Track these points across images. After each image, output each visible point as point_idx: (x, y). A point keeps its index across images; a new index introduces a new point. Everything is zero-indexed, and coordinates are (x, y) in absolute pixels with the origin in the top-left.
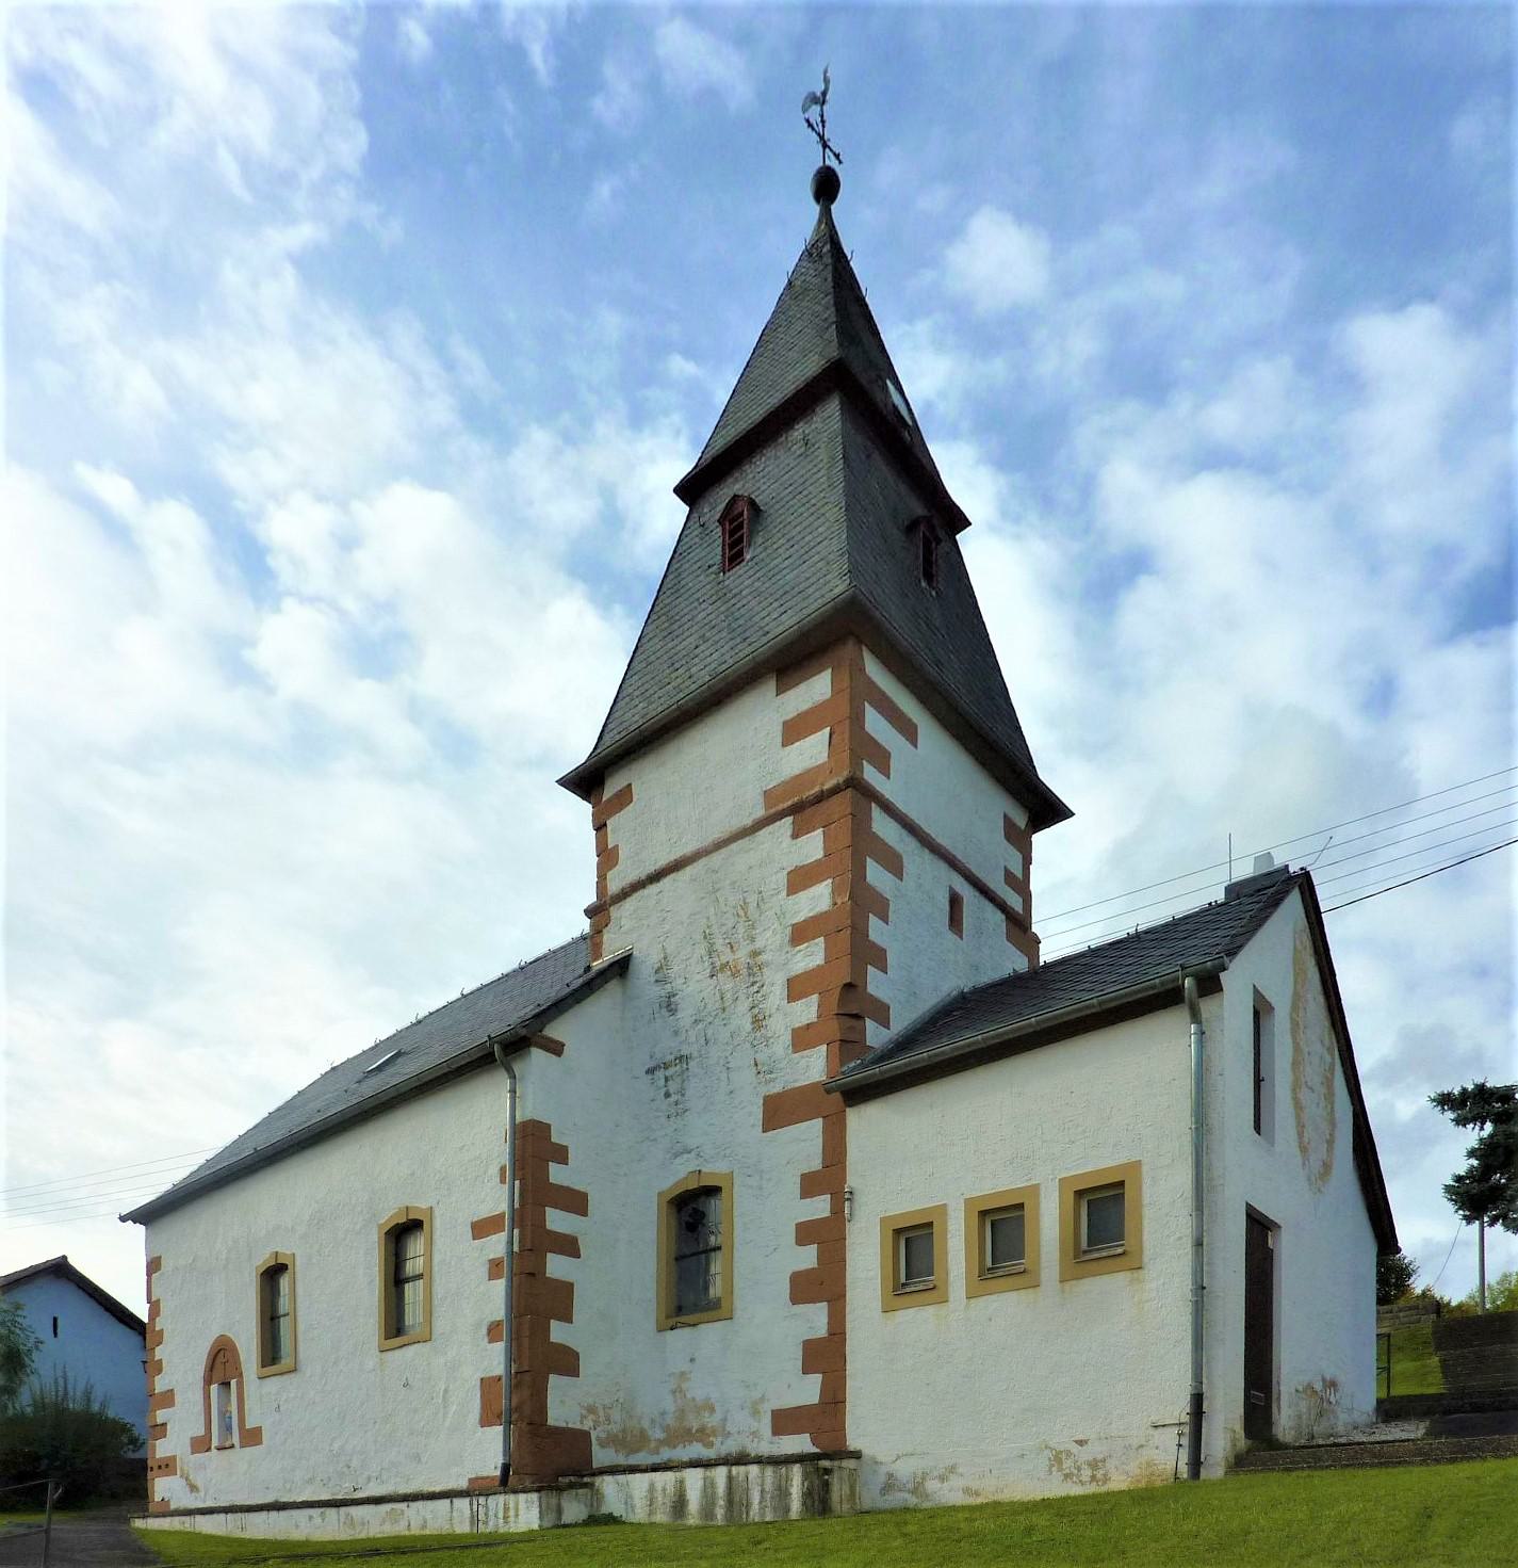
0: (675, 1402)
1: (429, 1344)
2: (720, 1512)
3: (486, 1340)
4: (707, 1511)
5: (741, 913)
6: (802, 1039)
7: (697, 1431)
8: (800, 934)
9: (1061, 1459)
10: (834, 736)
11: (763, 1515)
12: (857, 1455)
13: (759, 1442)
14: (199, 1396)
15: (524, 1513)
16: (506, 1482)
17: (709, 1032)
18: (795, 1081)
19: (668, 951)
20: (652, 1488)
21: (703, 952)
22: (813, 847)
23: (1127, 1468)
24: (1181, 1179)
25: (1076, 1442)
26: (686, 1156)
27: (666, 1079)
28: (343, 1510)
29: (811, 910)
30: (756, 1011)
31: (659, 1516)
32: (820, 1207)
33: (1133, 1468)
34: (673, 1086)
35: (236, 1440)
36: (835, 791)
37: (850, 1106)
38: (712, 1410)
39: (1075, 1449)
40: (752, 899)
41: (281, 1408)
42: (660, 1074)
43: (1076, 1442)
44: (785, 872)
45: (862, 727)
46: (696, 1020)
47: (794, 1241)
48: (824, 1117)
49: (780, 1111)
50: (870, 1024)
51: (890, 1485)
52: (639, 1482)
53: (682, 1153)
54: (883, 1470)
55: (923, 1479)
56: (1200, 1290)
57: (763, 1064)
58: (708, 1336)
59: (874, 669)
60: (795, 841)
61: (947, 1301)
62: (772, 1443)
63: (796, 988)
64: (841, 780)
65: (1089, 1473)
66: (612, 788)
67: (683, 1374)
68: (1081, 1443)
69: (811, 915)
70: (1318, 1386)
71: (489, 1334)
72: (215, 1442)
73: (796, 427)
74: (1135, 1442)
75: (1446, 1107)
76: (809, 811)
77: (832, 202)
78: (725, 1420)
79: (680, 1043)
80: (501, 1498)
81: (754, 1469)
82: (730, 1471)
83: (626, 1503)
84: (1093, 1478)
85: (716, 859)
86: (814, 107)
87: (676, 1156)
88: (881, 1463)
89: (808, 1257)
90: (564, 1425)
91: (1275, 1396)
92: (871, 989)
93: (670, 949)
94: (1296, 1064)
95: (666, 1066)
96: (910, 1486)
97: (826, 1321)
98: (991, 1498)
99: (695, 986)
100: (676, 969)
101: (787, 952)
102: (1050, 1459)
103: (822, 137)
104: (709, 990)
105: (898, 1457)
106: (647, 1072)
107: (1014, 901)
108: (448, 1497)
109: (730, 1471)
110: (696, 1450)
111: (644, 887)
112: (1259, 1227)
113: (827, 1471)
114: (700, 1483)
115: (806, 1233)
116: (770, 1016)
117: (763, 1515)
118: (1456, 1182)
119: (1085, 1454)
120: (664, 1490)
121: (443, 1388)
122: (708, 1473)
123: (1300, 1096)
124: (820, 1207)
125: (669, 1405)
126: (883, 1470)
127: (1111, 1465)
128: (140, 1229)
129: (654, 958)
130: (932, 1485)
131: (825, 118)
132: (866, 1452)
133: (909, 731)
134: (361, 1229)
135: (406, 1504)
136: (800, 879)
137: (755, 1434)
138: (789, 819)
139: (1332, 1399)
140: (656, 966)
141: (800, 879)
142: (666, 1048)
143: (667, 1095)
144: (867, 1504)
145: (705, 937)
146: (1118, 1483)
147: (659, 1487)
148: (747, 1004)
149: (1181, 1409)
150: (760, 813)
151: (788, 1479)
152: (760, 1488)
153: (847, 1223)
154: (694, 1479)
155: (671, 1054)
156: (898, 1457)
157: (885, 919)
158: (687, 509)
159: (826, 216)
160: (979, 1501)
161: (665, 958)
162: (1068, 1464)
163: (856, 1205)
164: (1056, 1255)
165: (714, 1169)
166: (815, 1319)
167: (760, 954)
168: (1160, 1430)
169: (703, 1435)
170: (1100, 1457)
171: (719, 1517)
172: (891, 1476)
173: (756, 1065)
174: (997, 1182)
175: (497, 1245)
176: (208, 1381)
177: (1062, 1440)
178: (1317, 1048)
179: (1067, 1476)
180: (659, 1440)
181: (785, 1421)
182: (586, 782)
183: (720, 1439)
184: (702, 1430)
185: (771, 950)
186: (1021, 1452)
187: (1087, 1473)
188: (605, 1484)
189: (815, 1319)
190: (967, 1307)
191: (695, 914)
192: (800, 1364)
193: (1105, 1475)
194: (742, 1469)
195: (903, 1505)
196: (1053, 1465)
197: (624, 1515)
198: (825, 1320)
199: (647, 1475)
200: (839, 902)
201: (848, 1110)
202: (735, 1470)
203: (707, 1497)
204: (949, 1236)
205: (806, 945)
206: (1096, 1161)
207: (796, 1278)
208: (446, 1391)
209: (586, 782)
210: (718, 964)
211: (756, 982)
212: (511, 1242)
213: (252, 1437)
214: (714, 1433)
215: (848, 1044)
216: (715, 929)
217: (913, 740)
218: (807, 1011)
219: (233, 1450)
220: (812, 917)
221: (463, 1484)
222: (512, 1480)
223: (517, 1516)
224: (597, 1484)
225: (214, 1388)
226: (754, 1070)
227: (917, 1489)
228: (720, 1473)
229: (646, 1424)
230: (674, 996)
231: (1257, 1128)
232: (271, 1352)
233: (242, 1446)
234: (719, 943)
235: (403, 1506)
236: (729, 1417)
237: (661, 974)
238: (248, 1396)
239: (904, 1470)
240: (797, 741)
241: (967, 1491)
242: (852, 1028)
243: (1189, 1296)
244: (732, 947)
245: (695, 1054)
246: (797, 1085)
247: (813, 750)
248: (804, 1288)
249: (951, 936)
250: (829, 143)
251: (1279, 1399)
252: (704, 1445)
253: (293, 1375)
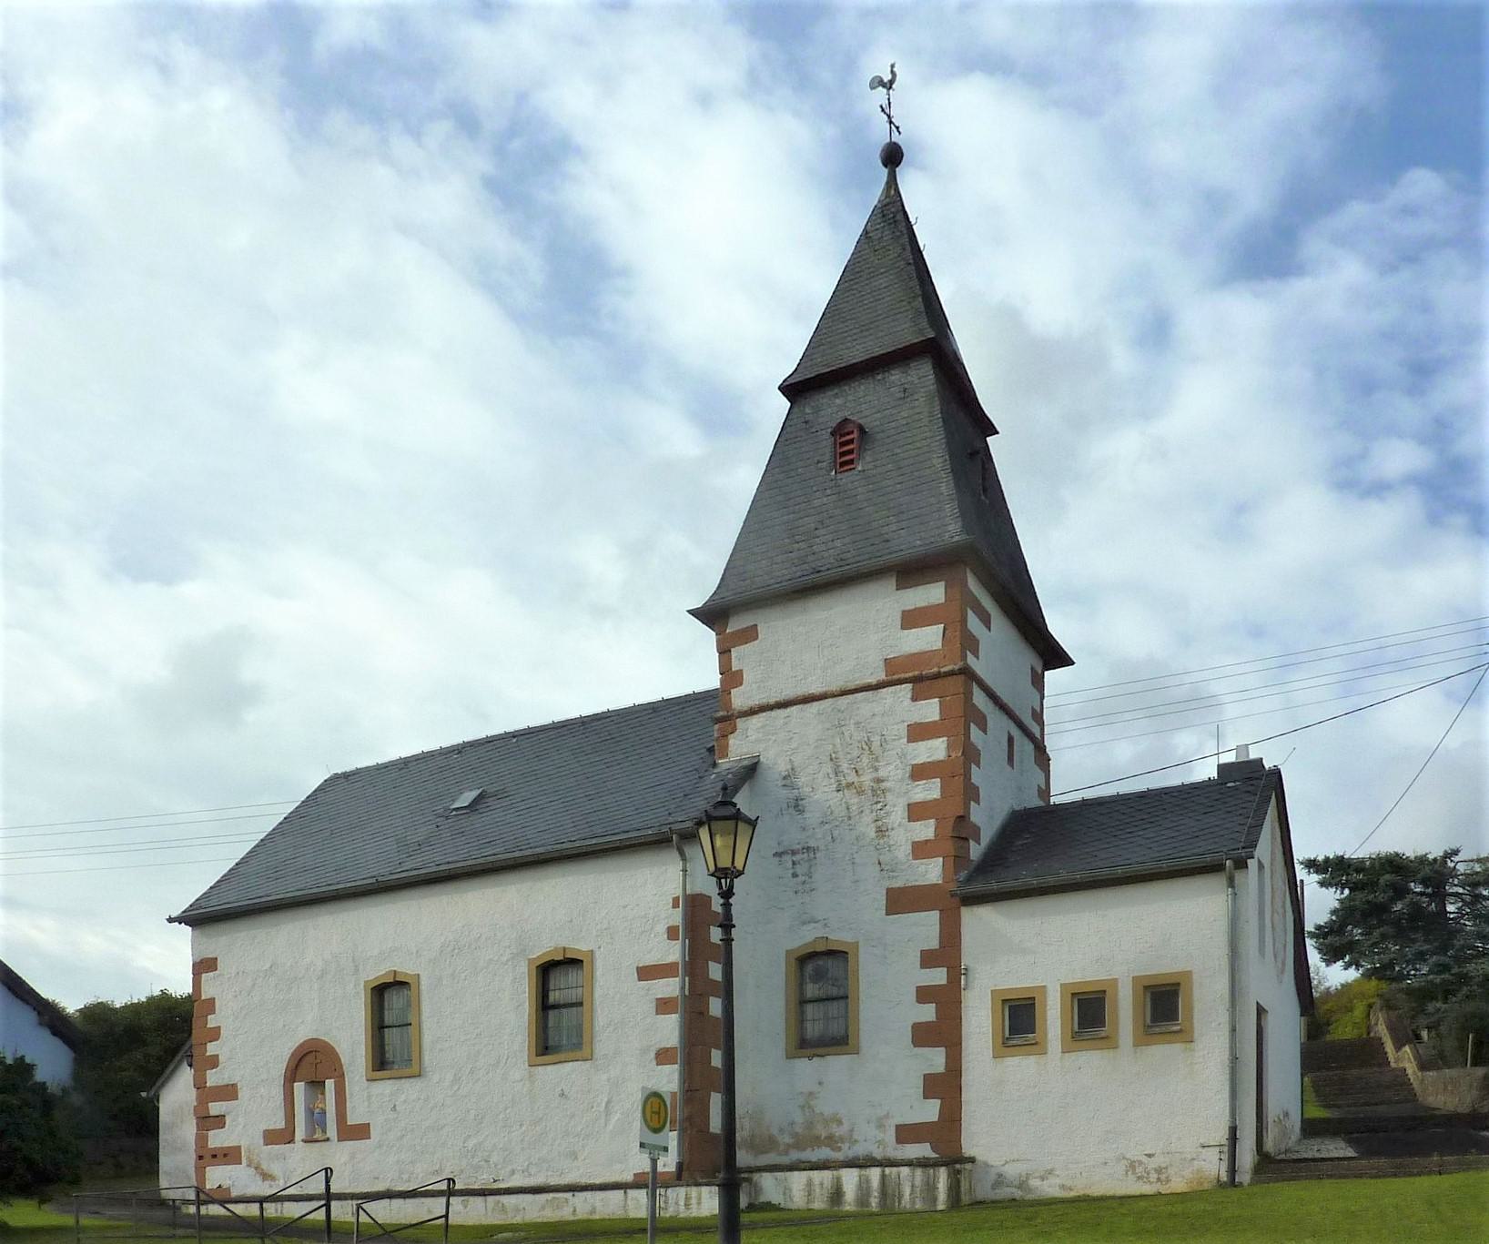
1: (589, 1063)
2: (874, 1202)
4: (863, 1199)
6: (921, 850)
7: (826, 1138)
9: (1135, 1166)
10: (947, 632)
11: (913, 1202)
12: (972, 1160)
14: (277, 1093)
15: (706, 1202)
16: (682, 1175)
17: (836, 833)
18: (916, 881)
19: (796, 764)
20: (810, 1183)
21: (830, 771)
22: (930, 710)
23: (1184, 1173)
24: (1222, 985)
25: (1146, 1155)
26: (813, 925)
27: (794, 863)
28: (490, 1199)
29: (928, 757)
30: (880, 823)
31: (816, 1204)
32: (938, 976)
33: (1187, 1173)
34: (799, 870)
35: (332, 1131)
36: (951, 673)
37: (965, 905)
38: (840, 1122)
39: (1145, 1159)
40: (876, 740)
41: (397, 1108)
42: (788, 859)
43: (1146, 1155)
44: (906, 724)
45: (966, 626)
46: (823, 822)
47: (915, 999)
49: (902, 901)
50: (972, 843)
51: (1000, 1181)
52: (798, 1180)
53: (809, 922)
54: (994, 1171)
56: (1234, 1060)
57: (886, 865)
58: (835, 1066)
59: (973, 584)
60: (914, 703)
61: (1045, 1053)
63: (916, 812)
64: (956, 667)
65: (1156, 1176)
66: (735, 625)
67: (811, 1094)
68: (1150, 1156)
69: (929, 760)
71: (656, 1058)
72: (300, 1133)
73: (893, 372)
74: (1189, 1157)
75: (1312, 870)
77: (897, 166)
79: (808, 837)
80: (682, 1191)
81: (905, 1171)
82: (883, 1171)
83: (784, 1194)
84: (1159, 1179)
85: (843, 701)
86: (880, 88)
87: (804, 923)
88: (992, 1166)
89: (928, 1013)
92: (973, 818)
93: (797, 760)
95: (794, 853)
96: (1016, 1183)
97: (944, 1061)
98: (1081, 1193)
99: (822, 793)
100: (802, 780)
101: (908, 785)
102: (1126, 1167)
103: (889, 116)
104: (835, 801)
105: (1007, 1162)
106: (775, 855)
107: (1036, 730)
108: (622, 1188)
109: (883, 1171)
110: (824, 1153)
111: (772, 709)
112: (1261, 1011)
113: (959, 1172)
114: (856, 1179)
116: (892, 829)
118: (1316, 929)
119: (1152, 1164)
120: (822, 1184)
121: (606, 1099)
122: (863, 1172)
124: (938, 976)
125: (799, 1118)
126: (994, 1171)
127: (1171, 1171)
128: (186, 930)
129: (783, 767)
130: (1034, 1183)
131: (891, 100)
132: (979, 1158)
133: (987, 622)
134: (508, 961)
135: (571, 1194)
136: (918, 732)
137: (880, 1143)
138: (910, 686)
140: (784, 774)
141: (918, 732)
142: (794, 838)
143: (795, 875)
144: (980, 1197)
145: (831, 759)
146: (1178, 1185)
147: (817, 1182)
149: (1222, 1135)
151: (935, 1178)
152: (910, 1184)
153: (962, 991)
154: (850, 1178)
155: (799, 844)
156: (1007, 1162)
157: (978, 765)
158: (789, 404)
159: (892, 182)
160: (1072, 1194)
161: (792, 769)
162: (1139, 1170)
163: (971, 979)
165: (840, 936)
167: (883, 781)
168: (1206, 1149)
169: (831, 1141)
170: (1164, 1165)
171: (874, 1205)
172: (1000, 1175)
174: (1086, 972)
175: (670, 987)
176: (292, 1075)
177: (1134, 1154)
178: (1280, 883)
181: (907, 1133)
182: (711, 615)
183: (847, 1145)
185: (893, 780)
186: (1104, 1161)
187: (1154, 1176)
188: (762, 1179)
190: (1061, 1058)
191: (821, 740)
193: (1167, 1178)
194: (895, 1169)
195: (1011, 1198)
197: (782, 1203)
199: (805, 1172)
200: (953, 755)
201: (962, 908)
202: (887, 1170)
203: (862, 1190)
204: (1048, 1008)
205: (924, 781)
206: (1163, 967)
208: (608, 1102)
209: (711, 615)
210: (844, 782)
211: (880, 802)
212: (683, 988)
213: (362, 1132)
214: (842, 1140)
215: (958, 860)
216: (841, 755)
217: (988, 625)
218: (925, 830)
219: (328, 1143)
220: (929, 762)
221: (629, 1178)
222: (685, 1174)
223: (699, 1203)
224: (755, 1179)
225: (299, 1088)
226: (878, 868)
227: (1022, 1185)
228: (874, 1174)
229: (775, 1131)
230: (802, 799)
232: (381, 1062)
234: (845, 766)
235: (568, 1195)
236: (856, 1129)
237: (788, 779)
238: (351, 1095)
239: (1012, 1171)
240: (915, 628)
241: (1063, 1187)
242: (961, 847)
243: (1227, 1062)
244: (856, 772)
245: (822, 847)
246: (917, 883)
247: (928, 638)
248: (923, 1036)
249: (1009, 768)
250: (893, 120)
252: (833, 1150)
253: (417, 1079)
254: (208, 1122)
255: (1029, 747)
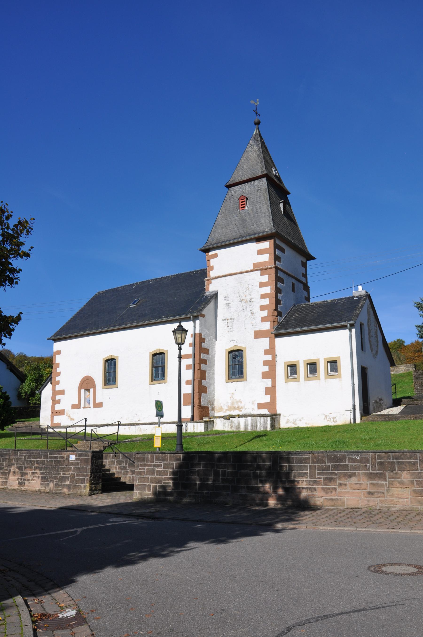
0: (231, 400)
3: (185, 384)
5: (248, 289)
6: (264, 319)
7: (237, 407)
8: (263, 296)
13: (254, 411)
27: (228, 323)
30: (252, 311)
35: (92, 405)
38: (241, 402)
39: (329, 415)
47: (263, 364)
48: (270, 338)
49: (258, 335)
55: (296, 420)
62: (258, 411)
63: (262, 308)
65: (333, 420)
68: (331, 413)
70: (378, 401)
76: (264, 270)
78: (245, 405)
84: (334, 421)
90: (204, 406)
91: (369, 404)
94: (369, 333)
95: (227, 320)
105: (290, 415)
107: (304, 280)
115: (265, 363)
117: (261, 429)
119: (332, 416)
123: (371, 339)
124: (269, 358)
139: (381, 403)
141: (262, 285)
143: (228, 326)
145: (238, 292)
148: (250, 309)
150: (252, 268)
155: (229, 317)
162: (328, 418)
164: (324, 373)
166: (268, 383)
169: (239, 408)
173: (252, 323)
179: (328, 420)
180: (226, 409)
181: (261, 406)
184: (238, 407)
189: (268, 383)
192: (264, 392)
196: (325, 418)
198: (271, 383)
207: (263, 373)
214: (242, 408)
225: (83, 391)
226: (252, 325)
228: (249, 419)
229: (222, 405)
231: (362, 350)
233: (94, 407)
248: (265, 376)
251: (370, 404)
254: (55, 402)
255: (301, 285)
